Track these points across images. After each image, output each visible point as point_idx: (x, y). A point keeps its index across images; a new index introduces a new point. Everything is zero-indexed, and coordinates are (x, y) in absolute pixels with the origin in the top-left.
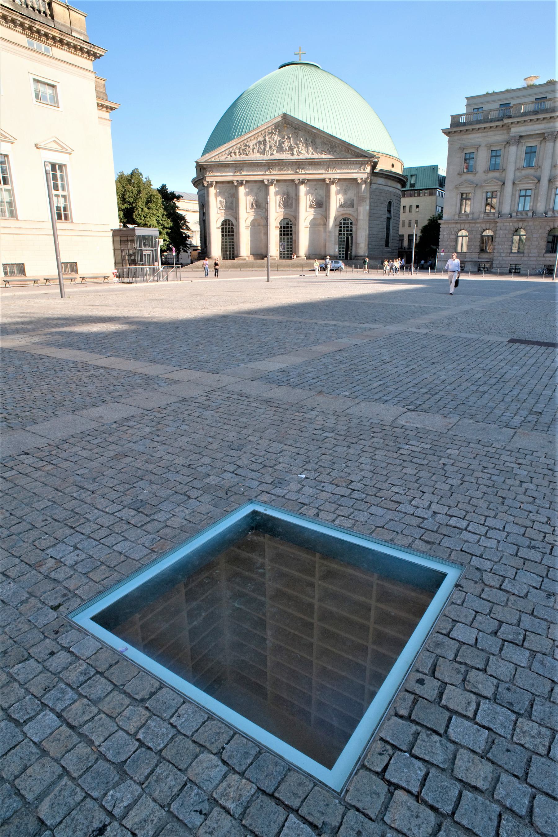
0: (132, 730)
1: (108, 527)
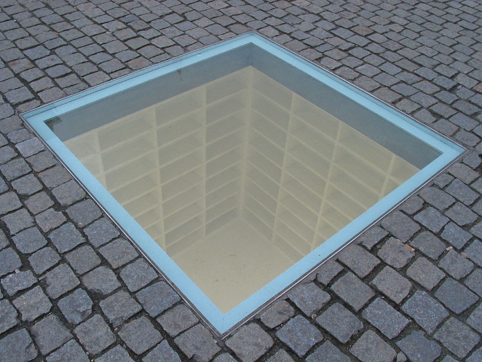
0: (46, 229)
1: (91, 37)
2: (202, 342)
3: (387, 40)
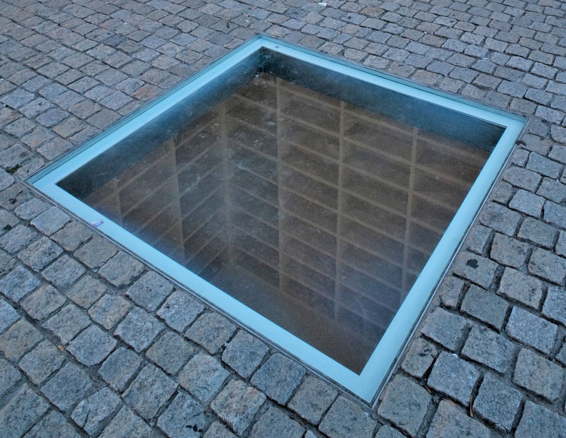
1: (78, 69)
2: (352, 419)
3: (401, 17)
